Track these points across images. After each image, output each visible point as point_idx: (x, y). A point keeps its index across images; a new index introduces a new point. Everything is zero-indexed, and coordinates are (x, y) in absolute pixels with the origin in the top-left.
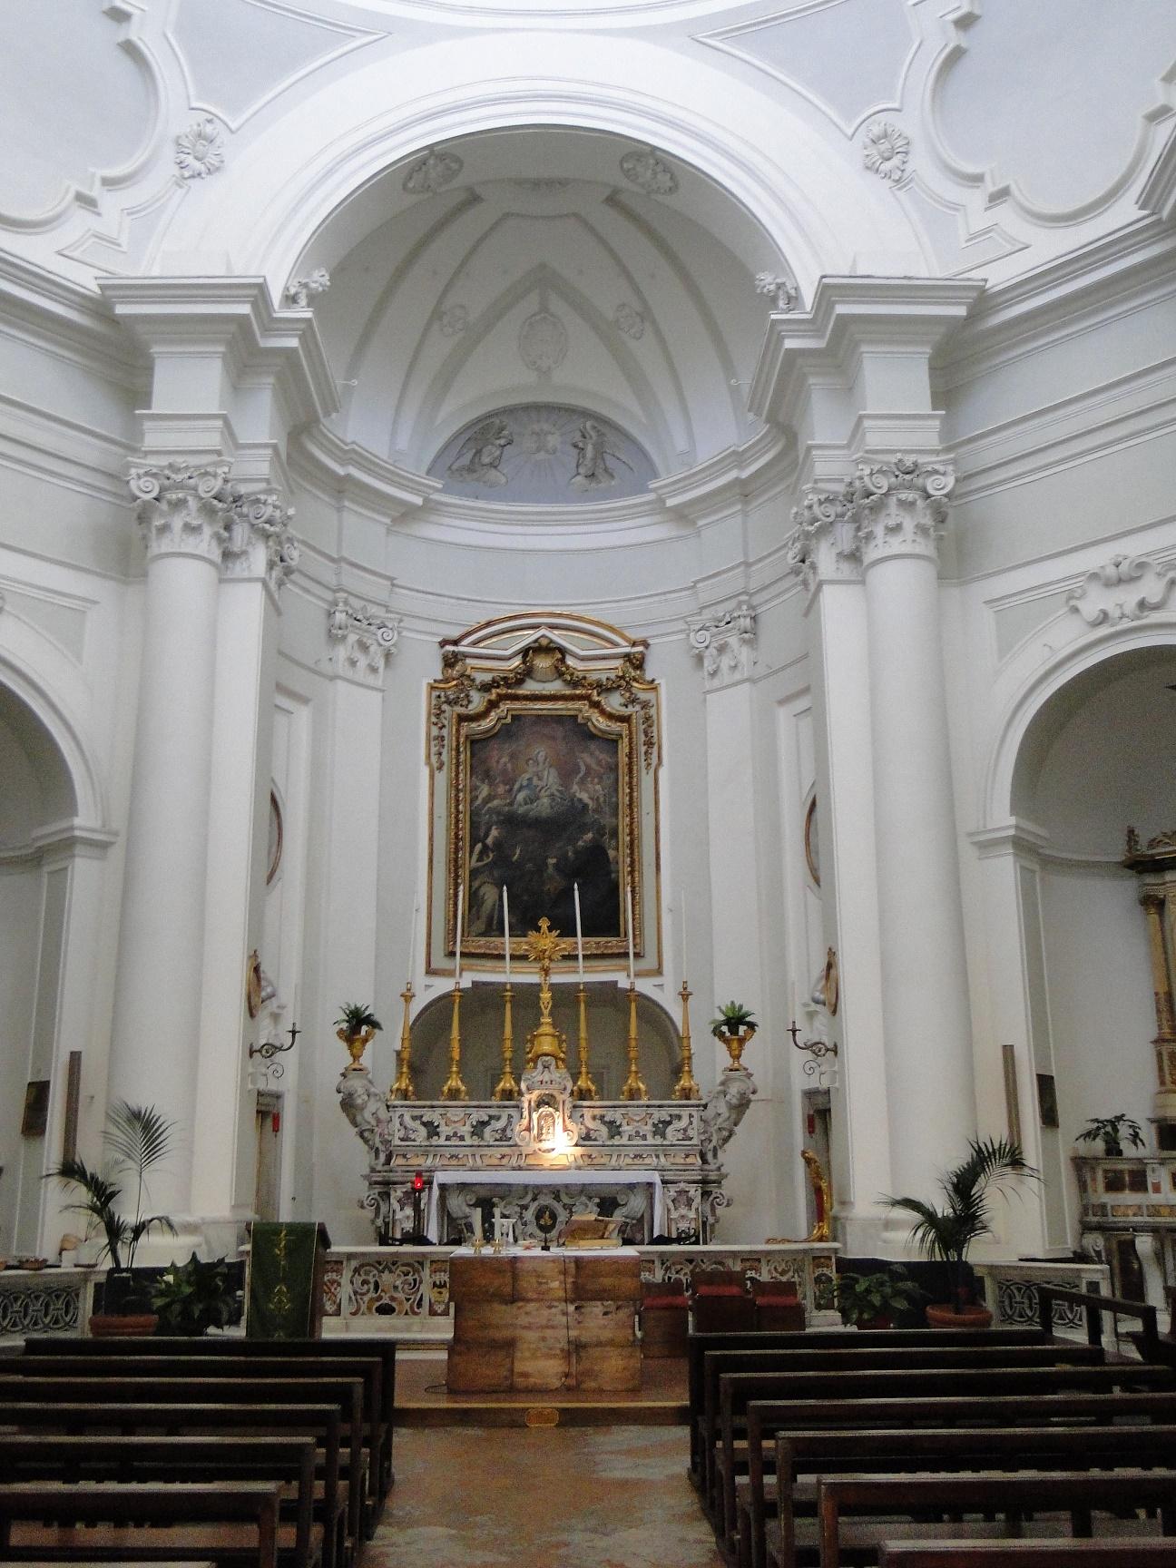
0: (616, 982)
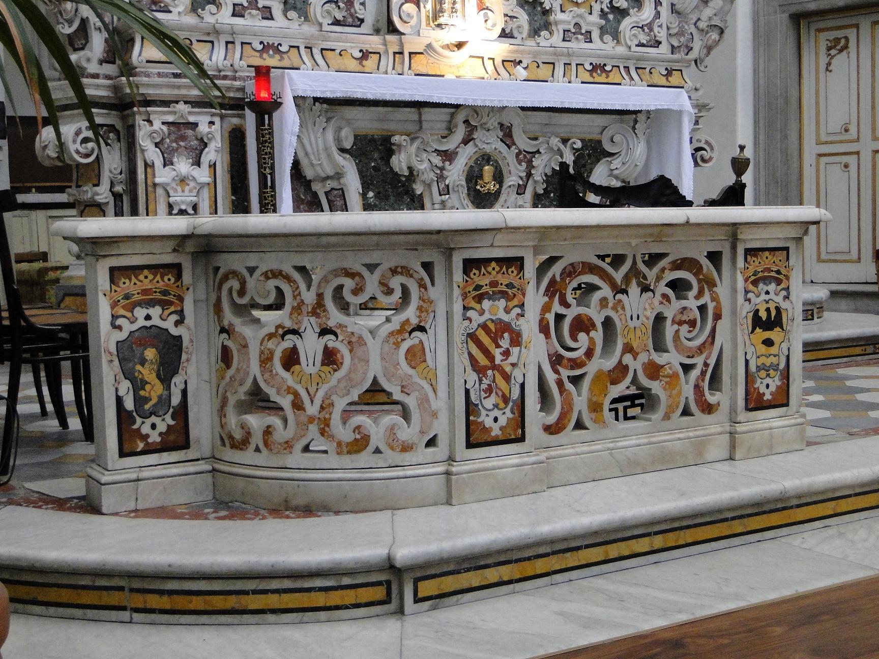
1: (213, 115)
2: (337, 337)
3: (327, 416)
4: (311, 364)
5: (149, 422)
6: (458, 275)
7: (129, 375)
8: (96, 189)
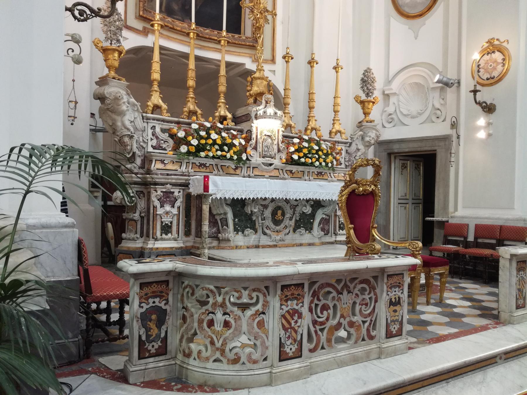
0: (243, 64)
1: (180, 189)
2: (230, 316)
3: (224, 348)
4: (219, 325)
5: (151, 345)
6: (279, 292)
7: (144, 326)
8: (134, 215)
